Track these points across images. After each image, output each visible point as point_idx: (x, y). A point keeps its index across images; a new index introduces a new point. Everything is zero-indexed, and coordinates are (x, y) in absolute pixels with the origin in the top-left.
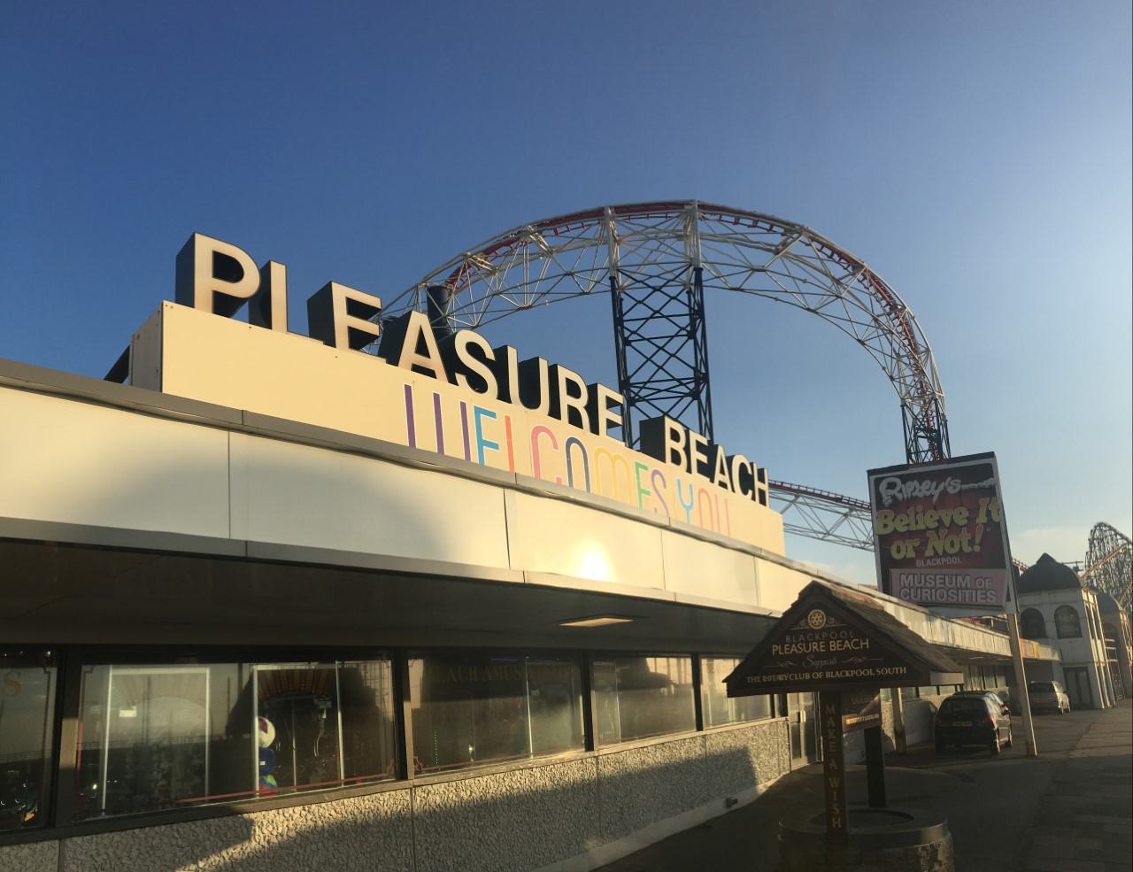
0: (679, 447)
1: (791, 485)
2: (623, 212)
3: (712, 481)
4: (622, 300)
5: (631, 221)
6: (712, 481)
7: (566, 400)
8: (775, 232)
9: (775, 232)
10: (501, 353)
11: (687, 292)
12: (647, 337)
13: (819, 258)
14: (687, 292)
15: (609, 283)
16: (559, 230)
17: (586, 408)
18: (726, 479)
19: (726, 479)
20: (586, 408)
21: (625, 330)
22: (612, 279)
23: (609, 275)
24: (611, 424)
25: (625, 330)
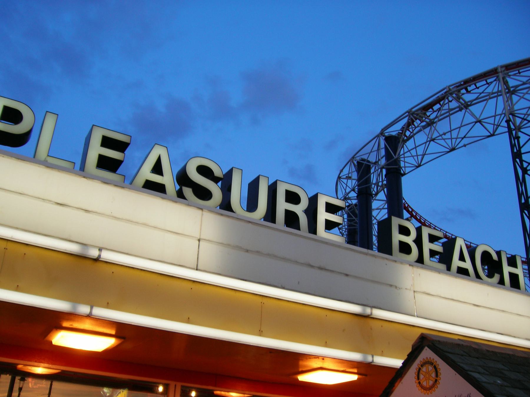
0: (409, 240)
1: (471, 243)
2: (493, 74)
3: (449, 269)
4: (519, 137)
5: (522, 74)
6: (449, 269)
7: (282, 206)
8: (491, 83)
9: (491, 83)
10: (229, 176)
11: (506, 121)
12: (370, 151)
13: (483, 93)
14: (506, 121)
15: (505, 125)
16: (469, 89)
17: (415, 241)
18: (467, 265)
19: (467, 265)
20: (306, 212)
21: (524, 162)
22: (508, 122)
23: (505, 119)
24: (433, 253)
25: (524, 163)
